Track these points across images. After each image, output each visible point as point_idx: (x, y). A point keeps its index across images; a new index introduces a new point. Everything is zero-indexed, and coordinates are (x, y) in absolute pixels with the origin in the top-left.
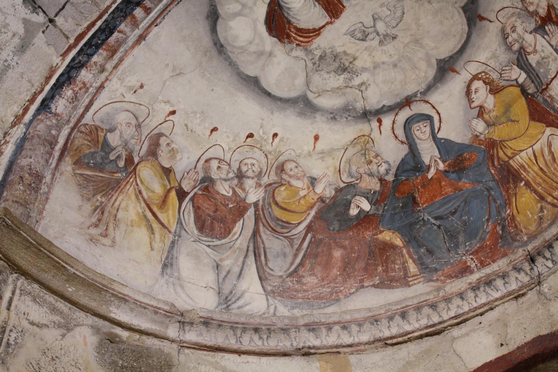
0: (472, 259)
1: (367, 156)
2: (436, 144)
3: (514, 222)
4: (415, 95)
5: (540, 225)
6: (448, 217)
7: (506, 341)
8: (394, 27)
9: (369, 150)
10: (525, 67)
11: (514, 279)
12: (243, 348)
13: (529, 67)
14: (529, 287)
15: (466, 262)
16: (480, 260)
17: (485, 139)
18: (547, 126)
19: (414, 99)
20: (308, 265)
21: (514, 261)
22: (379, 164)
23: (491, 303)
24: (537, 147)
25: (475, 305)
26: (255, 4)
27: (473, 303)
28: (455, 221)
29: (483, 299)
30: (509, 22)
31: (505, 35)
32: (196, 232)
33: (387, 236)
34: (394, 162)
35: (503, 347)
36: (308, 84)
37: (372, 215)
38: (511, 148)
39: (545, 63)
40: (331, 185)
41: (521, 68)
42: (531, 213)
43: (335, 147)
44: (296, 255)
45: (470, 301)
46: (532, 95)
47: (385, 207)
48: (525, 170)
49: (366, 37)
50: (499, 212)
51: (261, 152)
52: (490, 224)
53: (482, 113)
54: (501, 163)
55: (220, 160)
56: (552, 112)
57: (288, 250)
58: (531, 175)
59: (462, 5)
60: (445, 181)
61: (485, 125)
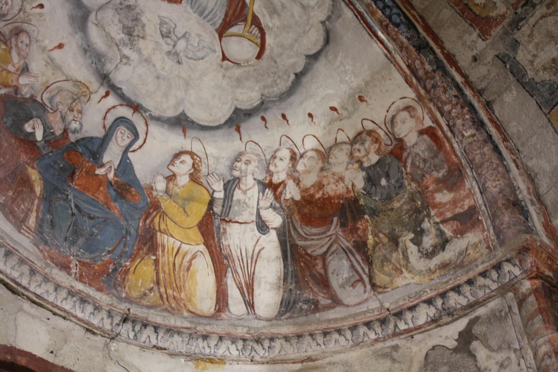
0: (76, 265)
1: (74, 104)
2: (122, 157)
3: (125, 275)
4: (146, 111)
5: (141, 298)
6: (84, 216)
7: (57, 352)
8: (187, 57)
9: (80, 101)
10: (228, 191)
11: (100, 317)
13: (230, 196)
14: (104, 333)
15: (70, 262)
16: (82, 273)
17: (155, 197)
18: (204, 244)
19: (142, 111)
21: (114, 307)
22: (76, 119)
23: (70, 315)
24: (185, 247)
25: (59, 304)
27: (59, 301)
28: (87, 224)
29: (67, 306)
30: (250, 155)
31: (238, 158)
33: (34, 175)
34: (86, 131)
35: (51, 354)
37: (38, 147)
38: (167, 226)
39: (243, 207)
40: (33, 89)
41: (225, 189)
42: (142, 283)
43: (63, 69)
45: (58, 297)
46: (214, 214)
47: (50, 152)
48: (163, 251)
49: (167, 37)
50: (121, 256)
51: (21, 4)
52: (108, 256)
53: (171, 180)
54: (152, 226)
56: (216, 239)
58: (165, 259)
59: (239, 107)
60: (104, 189)
61: (164, 189)
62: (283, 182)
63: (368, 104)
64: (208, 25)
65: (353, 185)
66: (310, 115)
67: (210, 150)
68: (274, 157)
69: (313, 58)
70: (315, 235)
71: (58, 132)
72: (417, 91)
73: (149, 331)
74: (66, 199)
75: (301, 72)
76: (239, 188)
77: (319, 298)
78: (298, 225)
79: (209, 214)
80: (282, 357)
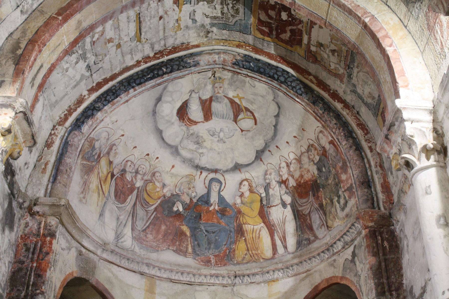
4: (220, 170)
12: (121, 265)
14: (230, 285)
15: (210, 258)
20: (150, 229)
24: (256, 227)
25: (209, 282)
26: (178, 101)
29: (212, 281)
32: (114, 198)
33: (185, 228)
36: (181, 142)
41: (265, 191)
44: (147, 221)
46: (264, 205)
48: (247, 233)
55: (132, 162)
57: (145, 217)
58: (248, 236)
59: (258, 149)
62: (287, 178)
63: (307, 132)
64: (228, 121)
65: (314, 173)
66: (287, 142)
67: (254, 174)
68: (280, 168)
69: (277, 116)
70: (305, 203)
71: (188, 202)
72: (321, 123)
73: (246, 278)
74: (201, 230)
75: (275, 124)
76: (271, 188)
77: (310, 237)
78: (297, 199)
79: (262, 206)
80: (298, 272)
